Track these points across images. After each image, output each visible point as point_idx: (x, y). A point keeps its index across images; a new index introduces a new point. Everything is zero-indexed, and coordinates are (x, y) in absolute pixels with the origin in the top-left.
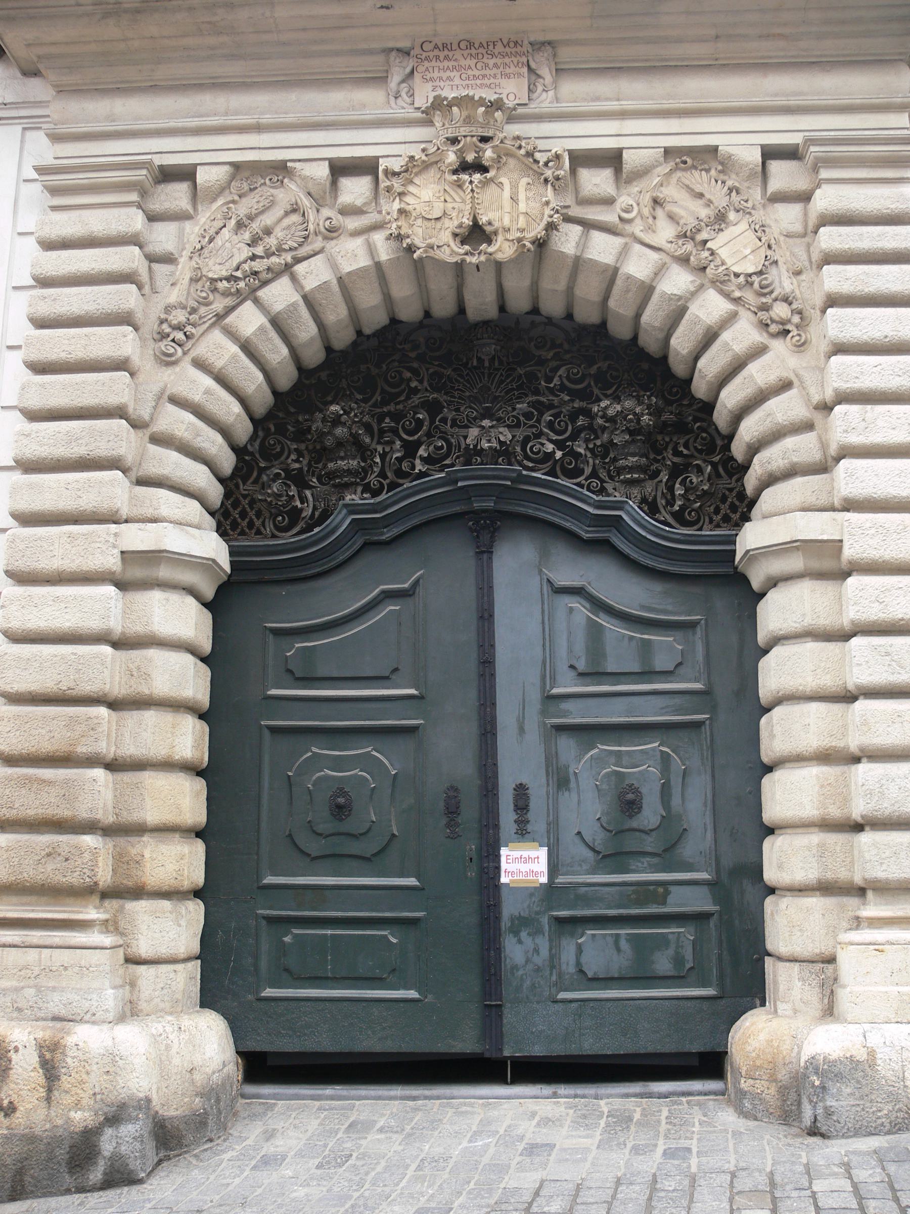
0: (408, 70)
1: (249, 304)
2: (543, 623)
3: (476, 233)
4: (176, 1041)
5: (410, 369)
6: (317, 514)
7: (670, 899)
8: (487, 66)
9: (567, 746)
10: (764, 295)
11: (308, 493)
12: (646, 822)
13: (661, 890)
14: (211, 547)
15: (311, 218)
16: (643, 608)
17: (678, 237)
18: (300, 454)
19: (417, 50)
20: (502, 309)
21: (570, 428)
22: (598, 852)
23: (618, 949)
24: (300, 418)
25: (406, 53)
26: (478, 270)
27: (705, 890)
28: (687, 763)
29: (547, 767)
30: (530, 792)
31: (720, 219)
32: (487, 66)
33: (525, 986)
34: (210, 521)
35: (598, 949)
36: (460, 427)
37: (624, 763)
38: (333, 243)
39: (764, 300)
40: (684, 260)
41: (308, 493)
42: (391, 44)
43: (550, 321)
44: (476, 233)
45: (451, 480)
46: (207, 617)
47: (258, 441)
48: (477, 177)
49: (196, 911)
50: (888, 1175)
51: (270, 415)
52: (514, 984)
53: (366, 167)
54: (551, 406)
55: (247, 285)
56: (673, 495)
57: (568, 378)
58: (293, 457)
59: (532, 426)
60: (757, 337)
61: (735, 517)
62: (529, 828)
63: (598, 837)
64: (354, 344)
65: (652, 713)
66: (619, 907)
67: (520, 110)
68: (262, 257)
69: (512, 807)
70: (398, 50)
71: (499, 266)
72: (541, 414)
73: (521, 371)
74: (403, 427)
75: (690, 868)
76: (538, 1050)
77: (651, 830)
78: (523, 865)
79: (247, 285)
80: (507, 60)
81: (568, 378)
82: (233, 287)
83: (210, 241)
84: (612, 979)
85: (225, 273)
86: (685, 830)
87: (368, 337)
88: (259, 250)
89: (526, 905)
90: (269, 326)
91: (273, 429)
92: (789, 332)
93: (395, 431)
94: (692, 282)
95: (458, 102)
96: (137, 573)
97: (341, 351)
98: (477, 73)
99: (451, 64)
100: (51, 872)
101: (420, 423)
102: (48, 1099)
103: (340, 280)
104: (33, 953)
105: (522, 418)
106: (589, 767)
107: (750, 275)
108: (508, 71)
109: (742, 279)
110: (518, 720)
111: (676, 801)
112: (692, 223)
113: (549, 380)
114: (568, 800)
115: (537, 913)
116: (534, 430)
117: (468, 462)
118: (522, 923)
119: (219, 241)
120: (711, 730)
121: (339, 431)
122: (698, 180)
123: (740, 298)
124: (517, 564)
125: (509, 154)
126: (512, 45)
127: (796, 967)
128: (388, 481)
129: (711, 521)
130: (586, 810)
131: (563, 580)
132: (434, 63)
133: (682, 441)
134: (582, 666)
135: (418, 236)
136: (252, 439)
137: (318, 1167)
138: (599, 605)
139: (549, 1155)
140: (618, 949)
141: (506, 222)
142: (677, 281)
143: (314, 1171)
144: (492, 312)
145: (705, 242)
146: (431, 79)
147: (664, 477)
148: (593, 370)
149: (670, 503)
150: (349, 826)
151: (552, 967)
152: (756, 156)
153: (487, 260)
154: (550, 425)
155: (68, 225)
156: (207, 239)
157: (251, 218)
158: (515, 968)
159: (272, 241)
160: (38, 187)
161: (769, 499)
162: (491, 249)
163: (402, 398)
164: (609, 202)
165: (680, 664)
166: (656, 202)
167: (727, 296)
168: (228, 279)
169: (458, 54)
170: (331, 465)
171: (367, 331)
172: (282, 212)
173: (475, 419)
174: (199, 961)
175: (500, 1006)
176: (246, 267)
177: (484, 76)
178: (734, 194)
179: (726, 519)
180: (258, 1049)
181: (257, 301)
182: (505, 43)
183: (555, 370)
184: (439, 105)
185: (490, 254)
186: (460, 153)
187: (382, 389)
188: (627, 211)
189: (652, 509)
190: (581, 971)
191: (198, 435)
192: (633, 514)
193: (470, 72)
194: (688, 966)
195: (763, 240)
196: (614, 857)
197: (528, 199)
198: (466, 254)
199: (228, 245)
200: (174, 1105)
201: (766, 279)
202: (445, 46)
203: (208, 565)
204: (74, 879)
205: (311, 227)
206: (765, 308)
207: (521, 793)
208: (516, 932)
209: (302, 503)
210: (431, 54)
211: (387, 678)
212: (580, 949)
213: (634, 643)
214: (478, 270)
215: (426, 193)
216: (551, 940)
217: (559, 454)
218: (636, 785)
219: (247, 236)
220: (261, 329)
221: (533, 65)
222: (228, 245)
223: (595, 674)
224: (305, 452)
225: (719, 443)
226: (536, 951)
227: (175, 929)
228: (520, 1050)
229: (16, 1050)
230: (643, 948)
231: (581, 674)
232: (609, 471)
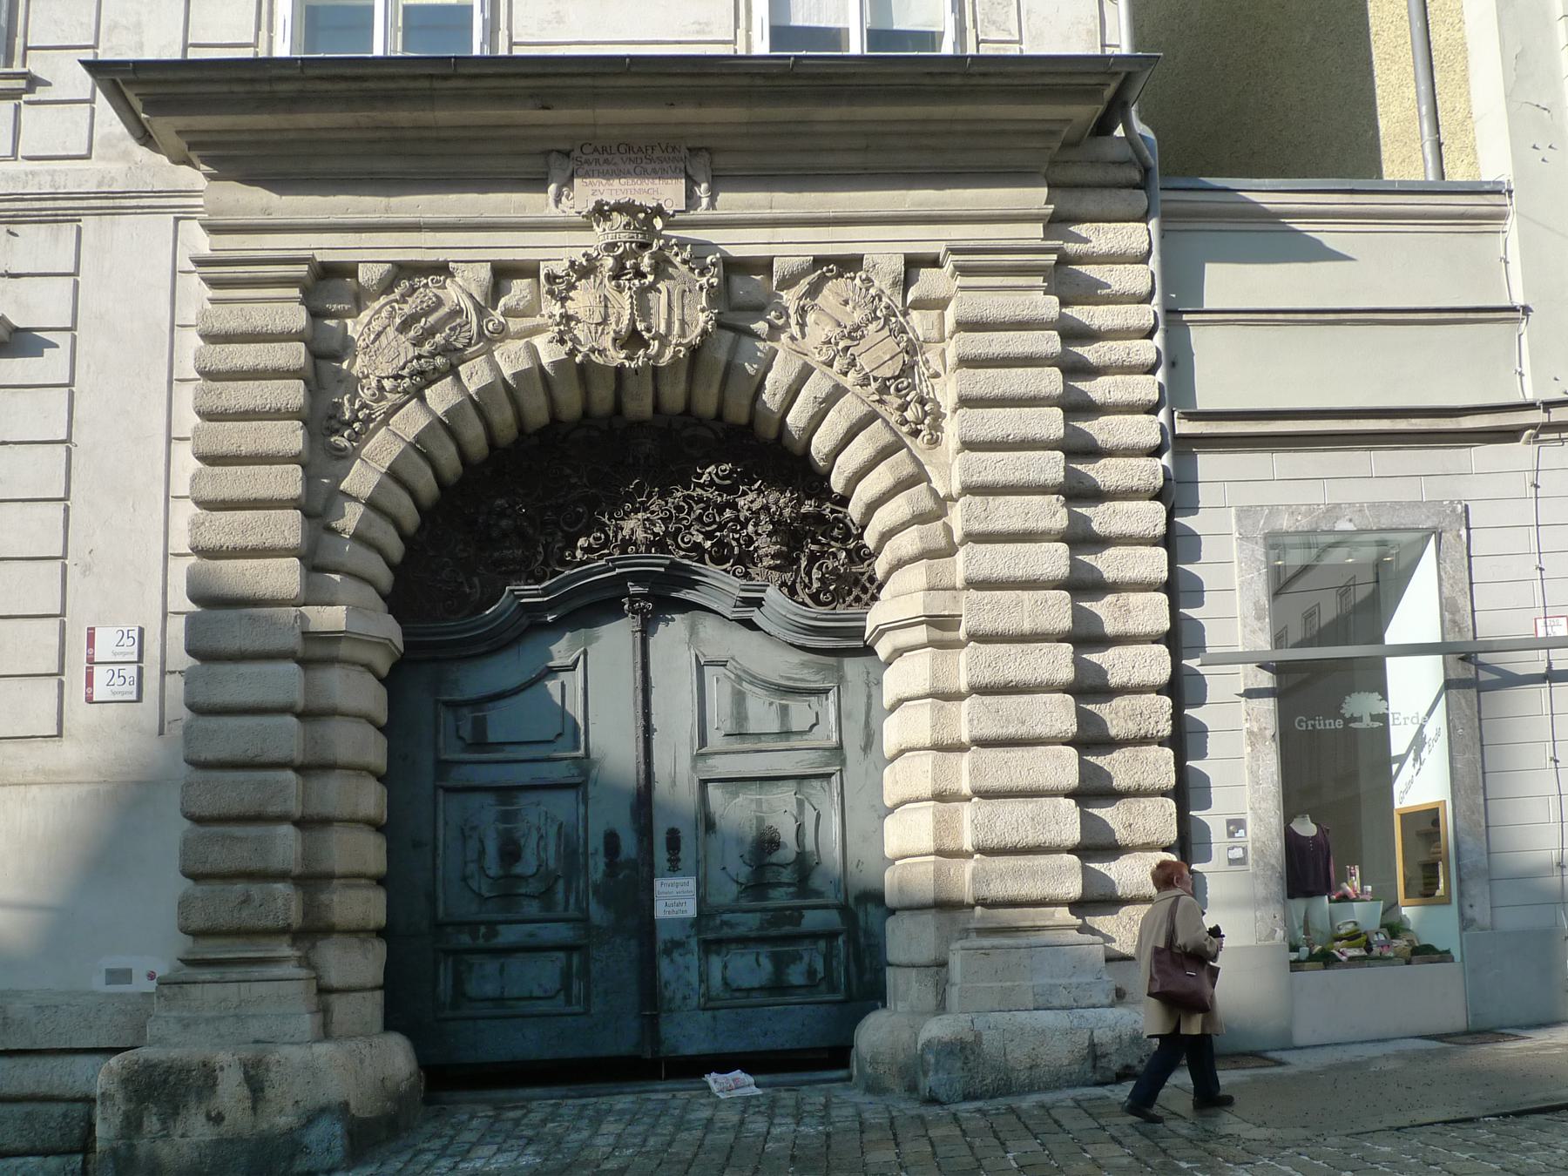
3: (632, 340)
7: (804, 921)
11: (476, 580)
14: (389, 629)
19: (577, 153)
25: (567, 154)
34: (381, 604)
35: (749, 968)
42: (550, 146)
43: (700, 421)
46: (382, 692)
49: (380, 949)
50: (694, 1068)
51: (438, 505)
53: (528, 270)
61: (865, 597)
62: (680, 865)
63: (744, 872)
64: (517, 442)
67: (678, 217)
80: (665, 165)
87: (529, 436)
95: (620, 208)
96: (319, 651)
100: (247, 917)
101: (579, 517)
102: (254, 1109)
104: (233, 986)
121: (504, 523)
127: (914, 971)
151: (701, 981)
152: (899, 265)
155: (230, 318)
160: (196, 278)
169: (617, 158)
170: (496, 554)
171: (530, 430)
179: (858, 599)
184: (601, 212)
200: (364, 1107)
203: (383, 644)
204: (269, 923)
208: (668, 952)
210: (591, 157)
212: (725, 967)
217: (708, 544)
221: (690, 172)
227: (357, 965)
229: (222, 1069)
230: (780, 963)
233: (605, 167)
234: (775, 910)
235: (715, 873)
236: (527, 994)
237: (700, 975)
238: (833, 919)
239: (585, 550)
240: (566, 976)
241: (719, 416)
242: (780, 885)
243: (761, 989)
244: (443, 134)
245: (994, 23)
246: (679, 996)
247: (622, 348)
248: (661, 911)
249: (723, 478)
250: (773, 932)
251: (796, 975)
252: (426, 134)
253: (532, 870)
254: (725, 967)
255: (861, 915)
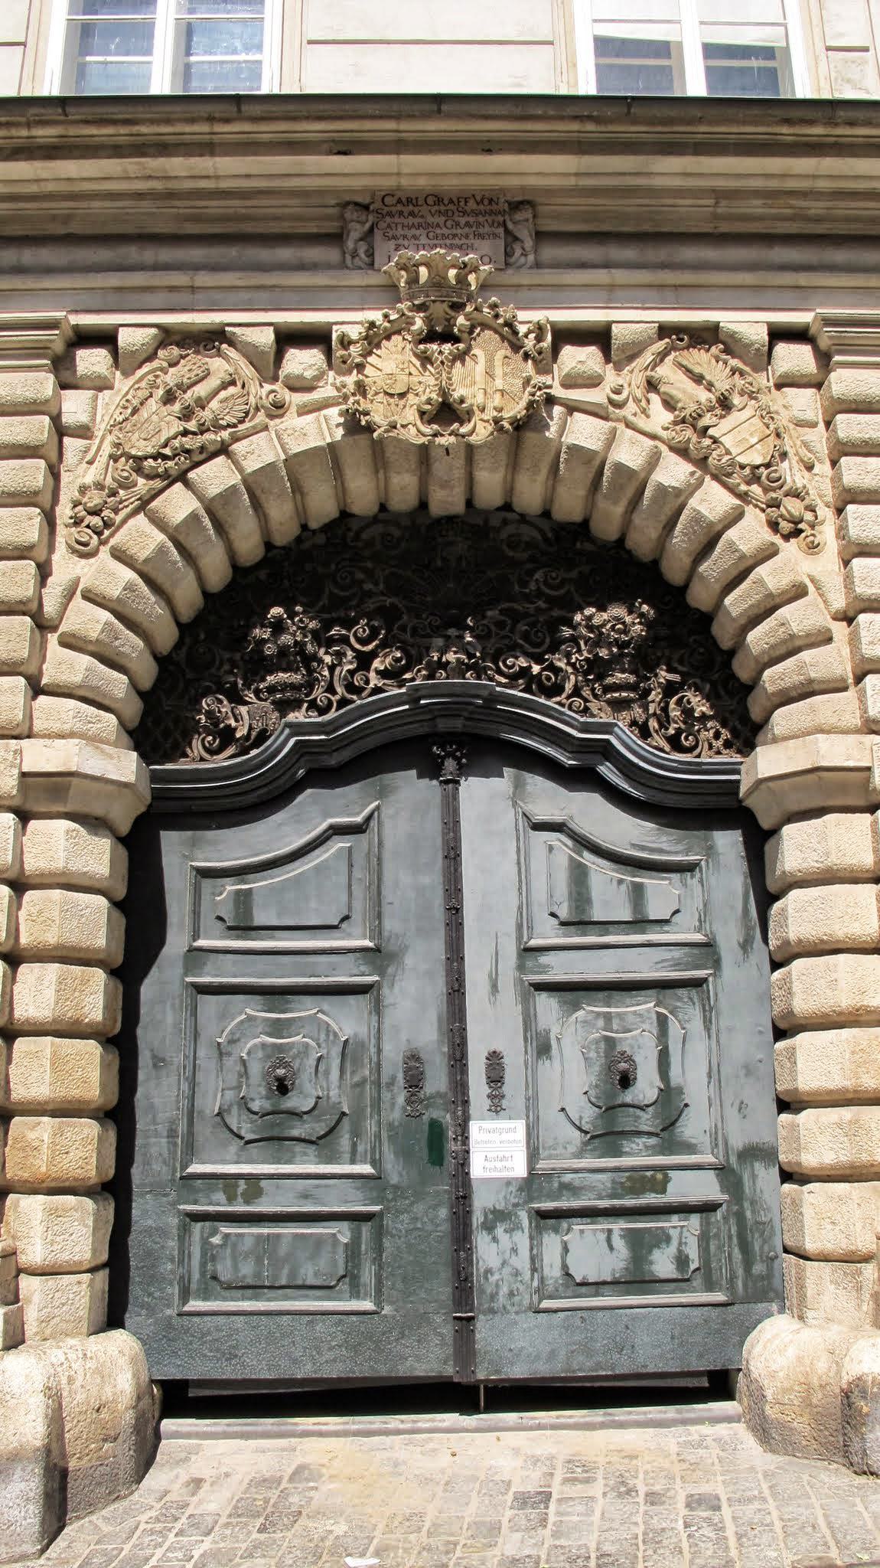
0: (367, 226)
1: (179, 485)
2: (519, 863)
4: (81, 1372)
5: (365, 570)
6: (254, 734)
8: (458, 224)
9: (546, 1004)
10: (774, 490)
12: (641, 1097)
13: (659, 1176)
14: (124, 766)
15: (253, 391)
16: (634, 846)
17: (675, 423)
18: (234, 664)
20: (469, 503)
21: (548, 640)
22: (586, 1133)
23: (611, 1248)
24: (236, 624)
26: (448, 454)
27: (711, 1175)
28: (687, 1026)
29: (525, 1031)
30: (505, 1060)
31: (725, 404)
32: (458, 224)
33: (501, 1293)
35: (594, 1251)
36: (423, 636)
37: (615, 1027)
38: (278, 421)
39: (774, 495)
40: (682, 451)
41: (243, 710)
43: (523, 518)
44: (447, 412)
45: (413, 698)
47: (184, 649)
48: (447, 347)
51: (200, 619)
52: (489, 1291)
54: (526, 615)
55: (176, 466)
56: (667, 716)
57: (545, 583)
58: (226, 667)
59: (504, 637)
60: (767, 535)
62: (505, 1103)
63: (588, 1114)
64: (299, 540)
65: (644, 966)
66: (612, 1196)
68: (194, 433)
69: (484, 1080)
70: (356, 204)
71: (470, 449)
72: (516, 622)
73: (491, 574)
74: (355, 635)
75: (690, 1149)
76: (518, 1371)
77: (648, 1106)
78: (496, 1150)
79: (176, 466)
80: (481, 219)
81: (545, 583)
82: (161, 466)
83: (133, 414)
84: (604, 1283)
85: (150, 450)
86: (686, 1105)
87: (314, 532)
88: (192, 425)
89: (501, 1196)
90: (202, 512)
91: (202, 636)
92: (801, 531)
93: (345, 640)
94: (692, 474)
97: (283, 548)
98: (445, 231)
99: (417, 221)
103: (245, 481)
105: (493, 628)
106: (573, 1032)
107: (758, 467)
108: (481, 230)
109: (747, 471)
110: (490, 976)
111: (675, 1072)
112: (692, 407)
113: (524, 584)
114: (549, 1070)
115: (516, 1205)
116: (507, 642)
117: (431, 676)
118: (497, 1217)
119: (144, 413)
120: (715, 988)
122: (701, 359)
123: (746, 493)
124: (485, 797)
125: (485, 326)
126: (486, 202)
128: (338, 697)
129: (711, 747)
130: (571, 1081)
131: (542, 815)
132: (397, 220)
133: (676, 656)
134: (564, 913)
135: (379, 414)
136: (178, 646)
137: (260, 1531)
138: (583, 843)
139: (547, 1508)
140: (611, 1248)
141: (480, 399)
142: (673, 472)
143: (255, 1535)
144: (458, 507)
145: (706, 428)
146: (394, 238)
147: (655, 696)
148: (574, 574)
149: (664, 724)
150: (292, 1102)
151: (534, 1270)
153: (458, 444)
154: (526, 636)
156: (129, 411)
157: (184, 388)
158: (489, 1271)
159: (206, 415)
161: (782, 719)
162: (463, 430)
163: (354, 603)
164: (594, 382)
165: (677, 911)
166: (652, 385)
167: (732, 490)
168: (155, 458)
169: (424, 210)
172: (219, 382)
173: (438, 628)
174: (107, 1271)
175: (472, 1318)
176: (176, 443)
177: (454, 236)
178: (737, 375)
180: (179, 1377)
181: (187, 484)
182: (478, 198)
183: (531, 573)
185: (463, 436)
186: (428, 320)
187: (331, 593)
188: (618, 392)
189: (645, 733)
190: (568, 1274)
191: (117, 639)
192: (623, 737)
193: (438, 231)
194: (693, 1267)
195: (772, 427)
196: (607, 1134)
197: (505, 374)
198: (435, 435)
199: (155, 418)
201: (776, 471)
202: (409, 201)
205: (252, 400)
206: (775, 504)
207: (495, 1060)
208: (489, 1227)
209: (237, 721)
210: (394, 209)
211: (335, 927)
212: (566, 1250)
213: (623, 887)
214: (448, 454)
215: (393, 362)
216: (531, 1238)
218: (629, 1053)
219: (177, 407)
220: (194, 517)
222: (155, 418)
223: (579, 923)
224: (241, 663)
225: (719, 659)
226: (514, 1250)
228: (497, 1372)
230: (641, 1245)
231: (563, 924)
232: (593, 690)
233: (411, 220)
234: (633, 1169)
235: (549, 1114)
236: (300, 1282)
237: (533, 1259)
238: (704, 1187)
239: (383, 674)
240: (353, 1252)
241: (546, 514)
242: (639, 1133)
243: (615, 1283)
244: (224, 185)
245: (849, 81)
246: (504, 1290)
247: (430, 422)
248: (478, 1169)
249: (551, 587)
250: (629, 1202)
251: (663, 1264)
252: (203, 184)
253: (307, 1105)
254: (566, 1250)
255: (746, 1177)
